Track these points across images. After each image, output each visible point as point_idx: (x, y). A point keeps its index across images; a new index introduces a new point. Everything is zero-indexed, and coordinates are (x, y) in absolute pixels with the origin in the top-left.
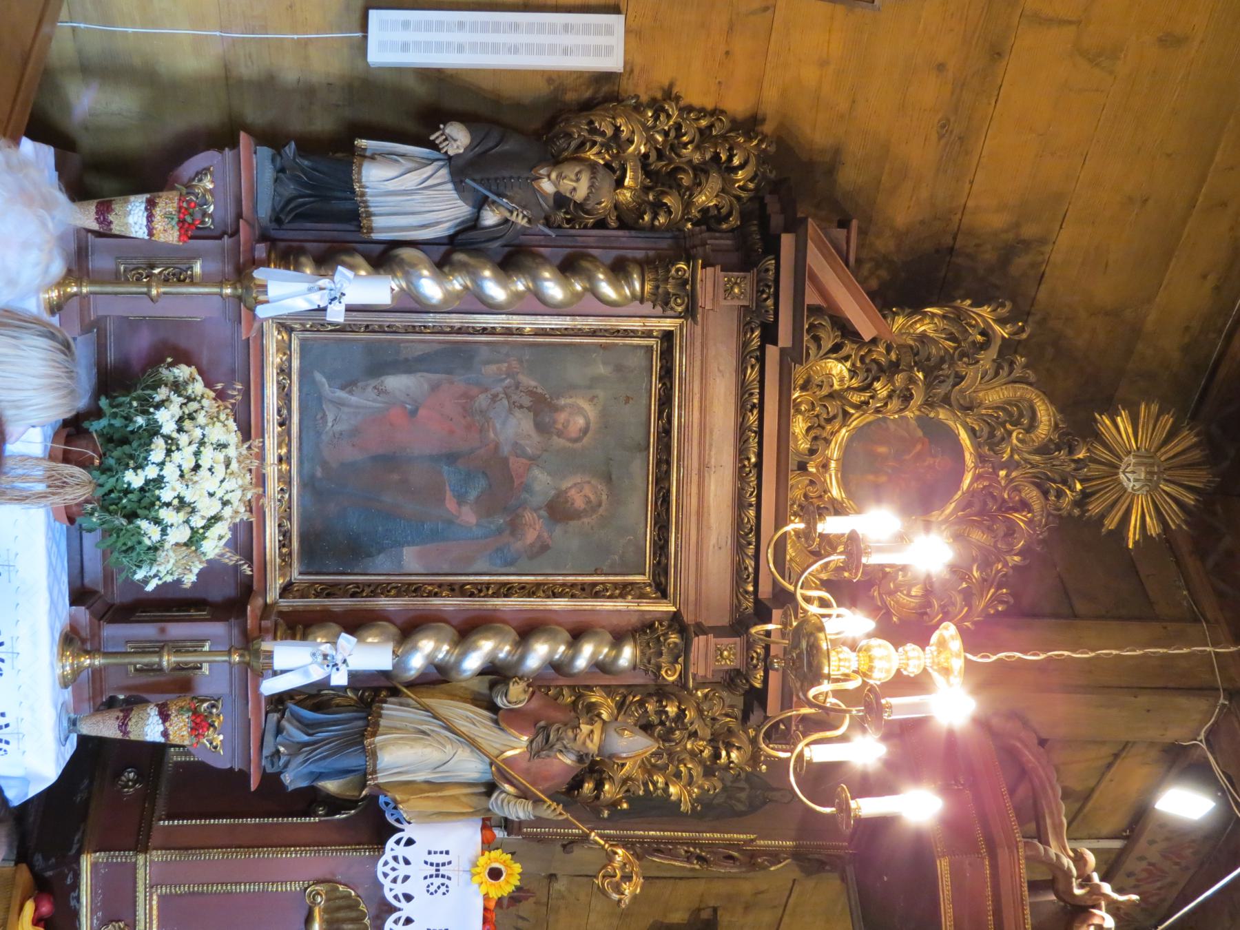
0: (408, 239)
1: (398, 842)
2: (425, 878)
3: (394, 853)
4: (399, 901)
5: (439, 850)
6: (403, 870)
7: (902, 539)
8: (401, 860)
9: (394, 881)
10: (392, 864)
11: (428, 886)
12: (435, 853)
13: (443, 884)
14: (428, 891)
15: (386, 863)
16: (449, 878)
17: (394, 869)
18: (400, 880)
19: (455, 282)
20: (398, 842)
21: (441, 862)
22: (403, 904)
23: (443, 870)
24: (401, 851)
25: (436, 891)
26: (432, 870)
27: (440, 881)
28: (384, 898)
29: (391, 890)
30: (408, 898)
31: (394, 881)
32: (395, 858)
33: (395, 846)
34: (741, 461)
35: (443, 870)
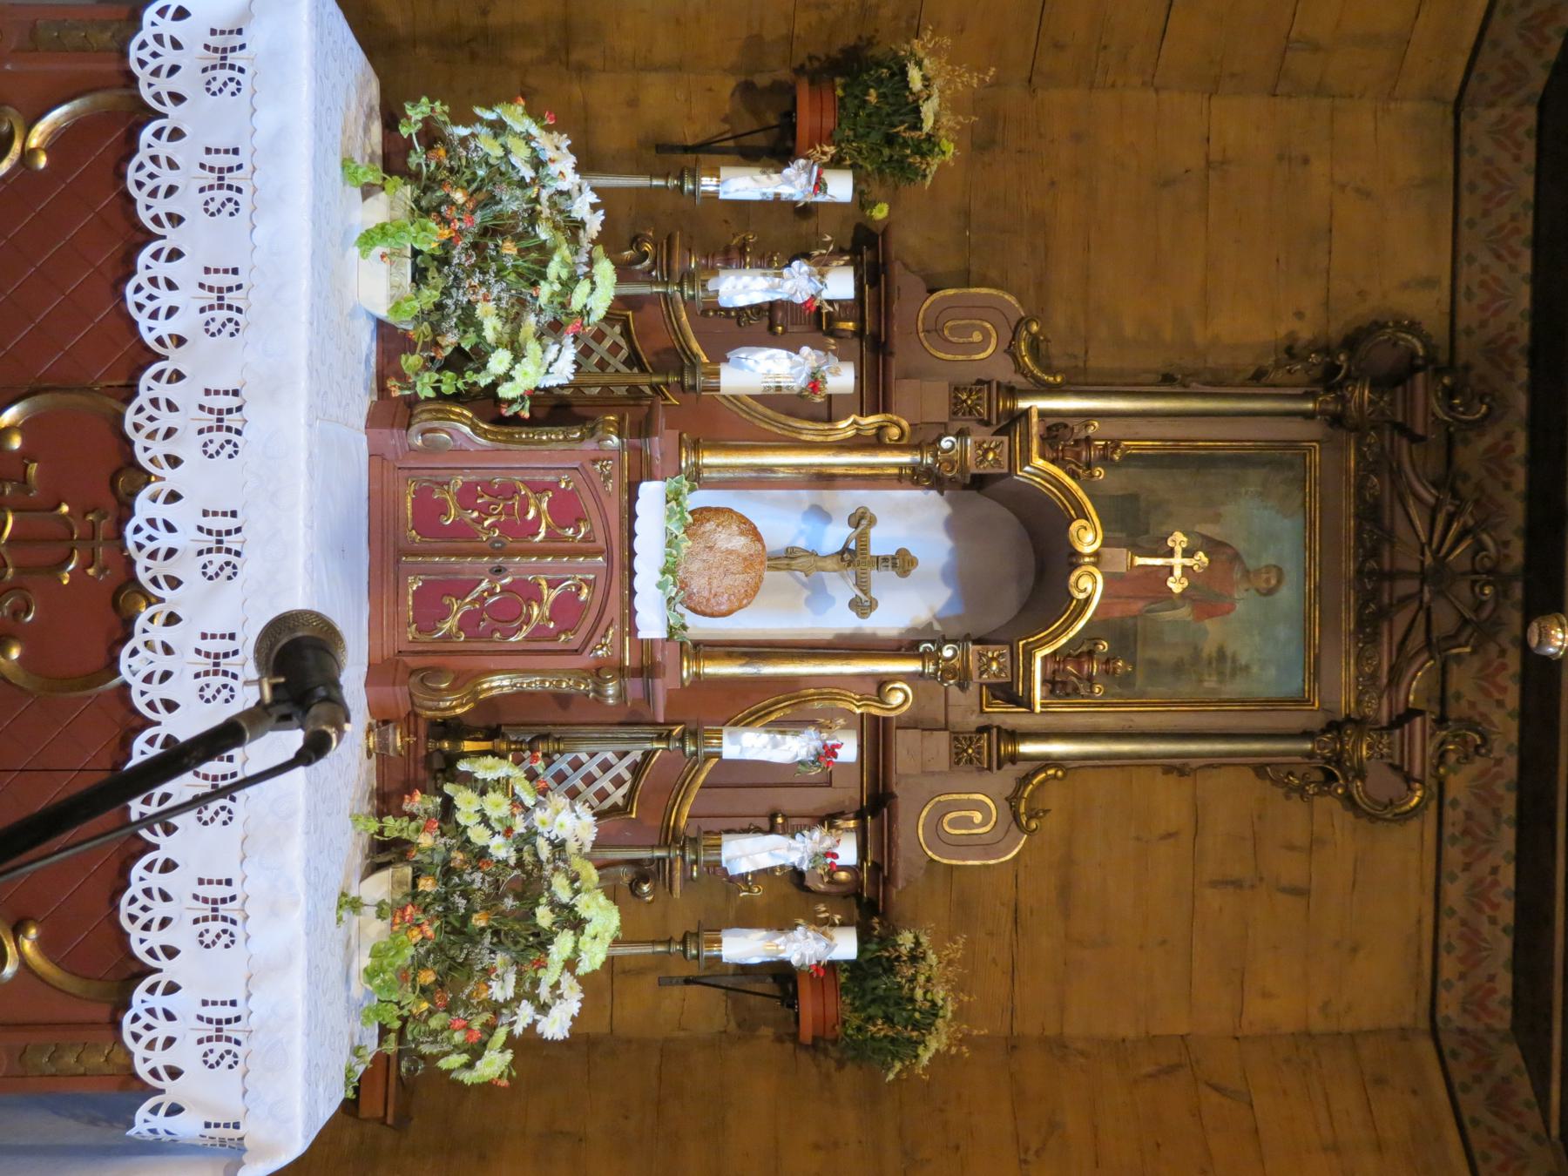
0: (896, 453)
1: (156, 256)
2: (202, 190)
3: (156, 30)
4: (159, 586)
5: (218, 633)
6: (163, 1029)
7: (830, 947)
8: (161, 282)
9: (151, 1046)
10: (143, 900)
11: (207, 323)
12: (217, 271)
13: (225, 686)
14: (202, 942)
15: (138, 289)
16: (239, 190)
17: (155, 55)
18: (159, 1044)
19: (409, 187)
20: (156, 256)
21: (226, 166)
22: (169, 108)
23: (229, 178)
24: (156, 880)
25: (218, 453)
26: (211, 420)
27: (224, 314)
28: (139, 98)
29: (147, 569)
30: (177, 98)
31: (151, 1046)
32: (147, 892)
33: (145, 874)
34: (832, 333)
35: (229, 178)
